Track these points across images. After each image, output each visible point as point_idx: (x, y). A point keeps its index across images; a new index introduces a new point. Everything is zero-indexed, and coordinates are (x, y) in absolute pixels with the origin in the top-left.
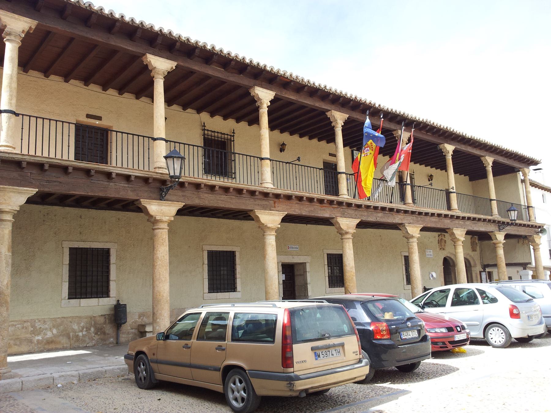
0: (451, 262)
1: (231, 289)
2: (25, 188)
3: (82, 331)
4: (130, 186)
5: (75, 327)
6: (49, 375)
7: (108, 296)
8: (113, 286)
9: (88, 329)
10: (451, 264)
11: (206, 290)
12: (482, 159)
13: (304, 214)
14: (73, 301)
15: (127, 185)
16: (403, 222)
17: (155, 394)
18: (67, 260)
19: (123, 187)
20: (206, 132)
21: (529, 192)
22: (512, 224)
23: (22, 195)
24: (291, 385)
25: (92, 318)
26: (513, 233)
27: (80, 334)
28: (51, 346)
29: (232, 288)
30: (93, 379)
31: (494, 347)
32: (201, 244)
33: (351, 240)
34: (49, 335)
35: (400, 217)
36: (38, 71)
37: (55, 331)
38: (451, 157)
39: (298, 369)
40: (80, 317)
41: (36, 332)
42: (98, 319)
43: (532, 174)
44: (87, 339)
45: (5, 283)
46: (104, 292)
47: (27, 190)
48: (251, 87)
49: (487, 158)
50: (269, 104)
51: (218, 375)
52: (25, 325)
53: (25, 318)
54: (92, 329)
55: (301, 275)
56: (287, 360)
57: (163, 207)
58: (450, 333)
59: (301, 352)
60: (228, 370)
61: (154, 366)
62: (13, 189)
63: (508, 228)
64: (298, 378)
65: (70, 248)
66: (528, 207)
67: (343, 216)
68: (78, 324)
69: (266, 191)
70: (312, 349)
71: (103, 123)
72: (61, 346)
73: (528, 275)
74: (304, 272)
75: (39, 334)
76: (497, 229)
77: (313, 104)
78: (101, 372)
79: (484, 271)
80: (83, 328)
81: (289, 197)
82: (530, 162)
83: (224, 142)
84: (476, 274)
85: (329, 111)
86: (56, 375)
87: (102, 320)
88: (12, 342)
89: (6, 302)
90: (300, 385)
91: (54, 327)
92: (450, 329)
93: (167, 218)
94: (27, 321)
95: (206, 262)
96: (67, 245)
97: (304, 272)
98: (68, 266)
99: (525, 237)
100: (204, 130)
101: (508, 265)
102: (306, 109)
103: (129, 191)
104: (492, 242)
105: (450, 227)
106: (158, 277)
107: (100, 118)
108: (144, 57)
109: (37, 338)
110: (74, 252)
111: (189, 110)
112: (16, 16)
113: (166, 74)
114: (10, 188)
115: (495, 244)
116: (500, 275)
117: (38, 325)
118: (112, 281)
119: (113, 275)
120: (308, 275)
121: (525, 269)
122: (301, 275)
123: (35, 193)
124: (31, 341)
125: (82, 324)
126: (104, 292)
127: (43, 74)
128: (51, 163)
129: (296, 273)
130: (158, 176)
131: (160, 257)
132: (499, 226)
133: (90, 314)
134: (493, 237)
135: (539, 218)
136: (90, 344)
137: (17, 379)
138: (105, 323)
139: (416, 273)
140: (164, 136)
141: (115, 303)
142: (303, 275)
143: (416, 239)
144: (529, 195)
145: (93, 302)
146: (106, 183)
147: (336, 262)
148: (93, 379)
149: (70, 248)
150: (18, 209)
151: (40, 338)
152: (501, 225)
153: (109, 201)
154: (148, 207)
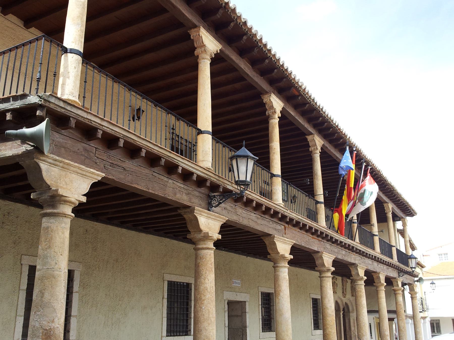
1: (183, 332)
2: (92, 170)
4: (185, 187)
11: (165, 333)
13: (303, 245)
15: (182, 186)
16: (357, 262)
19: (179, 187)
23: (85, 180)
32: (163, 272)
36: (18, 17)
47: (93, 173)
55: (237, 316)
62: (79, 168)
63: (406, 276)
65: (30, 266)
74: (242, 313)
77: (303, 124)
84: (354, 320)
85: (311, 134)
97: (242, 313)
98: (25, 292)
101: (369, 312)
102: (293, 127)
103: (184, 194)
104: (393, 288)
105: (378, 271)
106: (206, 316)
108: (193, 30)
114: (75, 167)
115: (395, 290)
116: (400, 322)
118: (74, 316)
122: (237, 316)
123: (100, 178)
127: (23, 22)
128: (129, 140)
131: (209, 288)
132: (399, 273)
134: (394, 283)
142: (241, 316)
143: (363, 282)
146: (166, 179)
147: (268, 302)
149: (30, 266)
153: (157, 203)
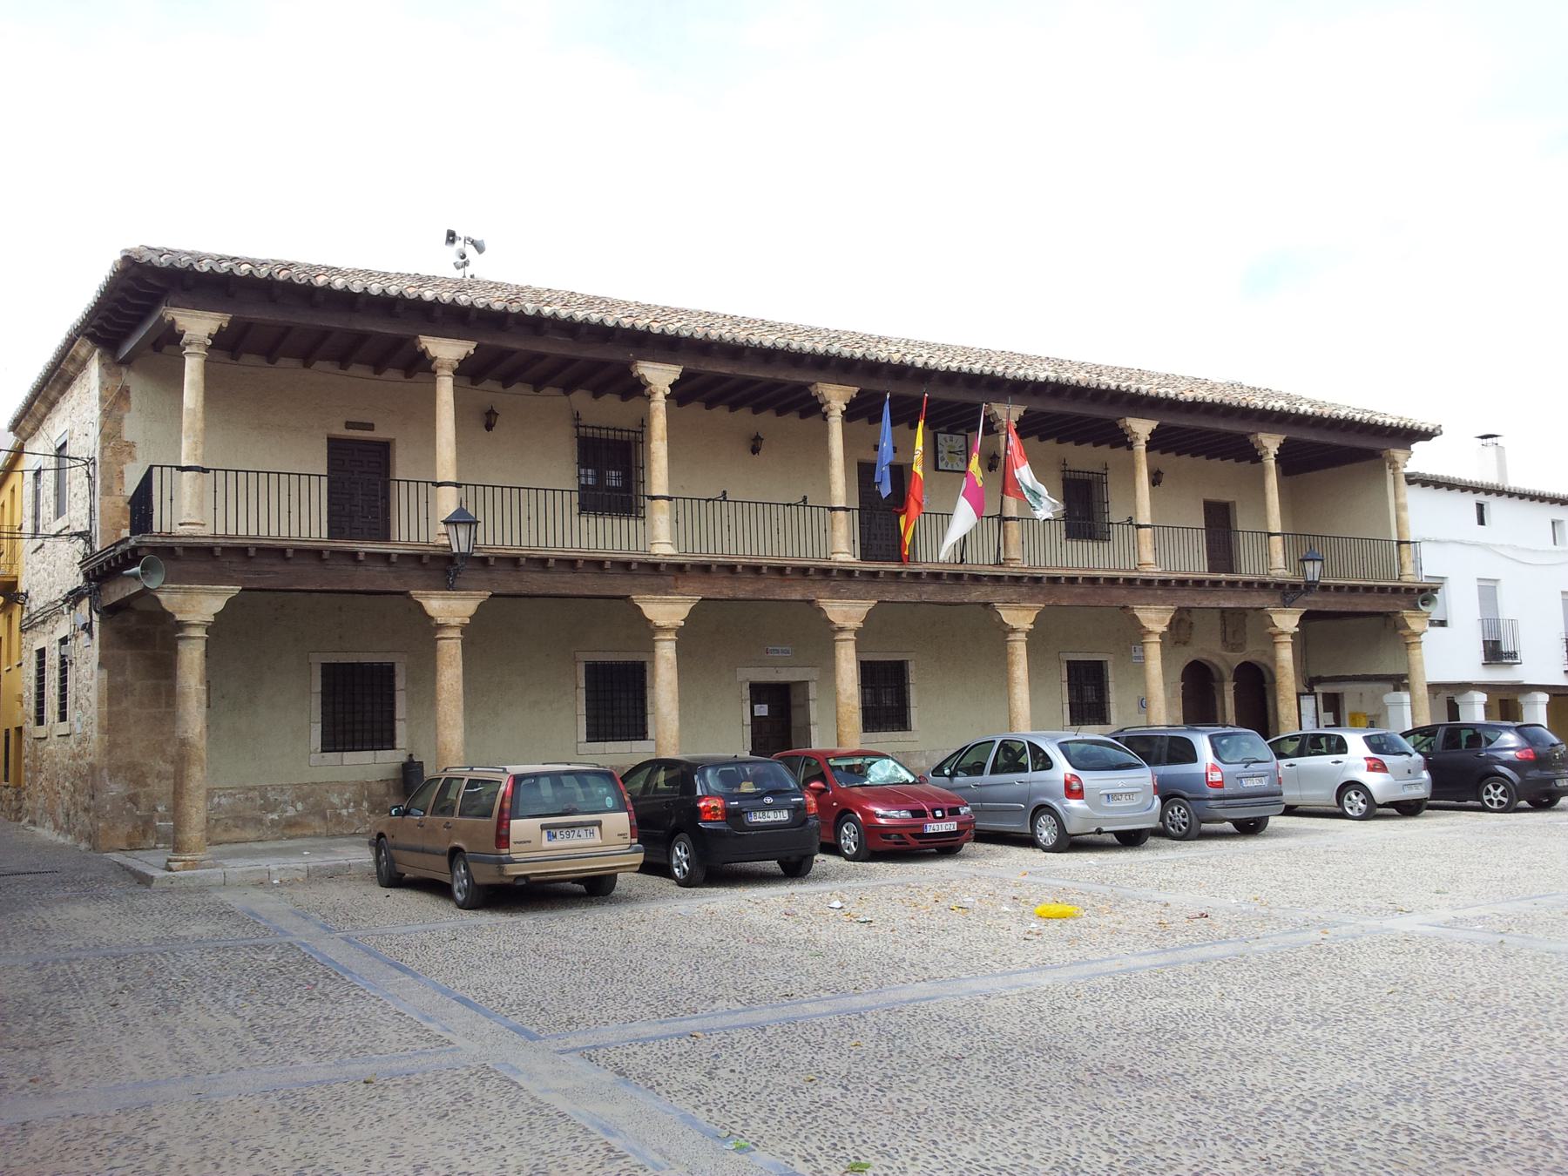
0: (1214, 670)
3: (347, 807)
5: (335, 800)
6: (264, 866)
7: (393, 748)
8: (401, 729)
9: (358, 804)
10: (1216, 676)
12: (1252, 439)
14: (332, 757)
17: (398, 895)
18: (317, 687)
20: (582, 430)
21: (1404, 507)
22: (1310, 586)
24: (501, 869)
25: (364, 785)
26: (1320, 607)
27: (344, 812)
28: (294, 832)
29: (1406, 676)
30: (333, 875)
31: (1046, 850)
33: (852, 644)
34: (291, 812)
35: (983, 589)
37: (300, 806)
38: (1143, 448)
39: (515, 851)
40: (343, 784)
41: (269, 807)
42: (375, 786)
43: (1420, 458)
44: (356, 822)
45: (197, 730)
46: (388, 742)
48: (632, 363)
49: (1261, 436)
50: (668, 391)
51: (445, 860)
52: (251, 794)
53: (251, 784)
54: (365, 804)
56: (502, 839)
57: (452, 602)
58: (918, 821)
59: (520, 827)
60: (455, 853)
61: (393, 852)
64: (512, 861)
66: (1399, 543)
67: (836, 595)
68: (341, 794)
69: (651, 559)
70: (543, 827)
71: (379, 434)
72: (310, 832)
73: (1401, 704)
75: (272, 812)
76: (1278, 600)
78: (343, 867)
79: (1311, 693)
80: (348, 802)
81: (705, 568)
82: (1408, 436)
83: (628, 443)
86: (273, 868)
87: (382, 789)
88: (230, 822)
89: (201, 759)
90: (512, 870)
91: (299, 798)
92: (918, 813)
93: (458, 620)
94: (254, 788)
95: (582, 684)
96: (318, 659)
99: (1386, 616)
100: (577, 427)
107: (370, 427)
109: (271, 816)
110: (329, 670)
111: (548, 390)
112: (199, 313)
113: (456, 365)
115: (1274, 635)
117: (271, 795)
119: (400, 712)
120: (813, 706)
121: (1397, 689)
124: (259, 822)
125: (347, 796)
126: (388, 742)
129: (794, 701)
130: (440, 551)
132: (1285, 594)
133: (360, 777)
135: (1430, 564)
136: (362, 830)
137: (219, 870)
138: (387, 795)
139: (1019, 703)
140: (453, 479)
141: (405, 759)
144: (1403, 514)
145: (366, 757)
148: (333, 875)
150: (212, 619)
151: (275, 816)
152: (1287, 592)
154: (424, 602)
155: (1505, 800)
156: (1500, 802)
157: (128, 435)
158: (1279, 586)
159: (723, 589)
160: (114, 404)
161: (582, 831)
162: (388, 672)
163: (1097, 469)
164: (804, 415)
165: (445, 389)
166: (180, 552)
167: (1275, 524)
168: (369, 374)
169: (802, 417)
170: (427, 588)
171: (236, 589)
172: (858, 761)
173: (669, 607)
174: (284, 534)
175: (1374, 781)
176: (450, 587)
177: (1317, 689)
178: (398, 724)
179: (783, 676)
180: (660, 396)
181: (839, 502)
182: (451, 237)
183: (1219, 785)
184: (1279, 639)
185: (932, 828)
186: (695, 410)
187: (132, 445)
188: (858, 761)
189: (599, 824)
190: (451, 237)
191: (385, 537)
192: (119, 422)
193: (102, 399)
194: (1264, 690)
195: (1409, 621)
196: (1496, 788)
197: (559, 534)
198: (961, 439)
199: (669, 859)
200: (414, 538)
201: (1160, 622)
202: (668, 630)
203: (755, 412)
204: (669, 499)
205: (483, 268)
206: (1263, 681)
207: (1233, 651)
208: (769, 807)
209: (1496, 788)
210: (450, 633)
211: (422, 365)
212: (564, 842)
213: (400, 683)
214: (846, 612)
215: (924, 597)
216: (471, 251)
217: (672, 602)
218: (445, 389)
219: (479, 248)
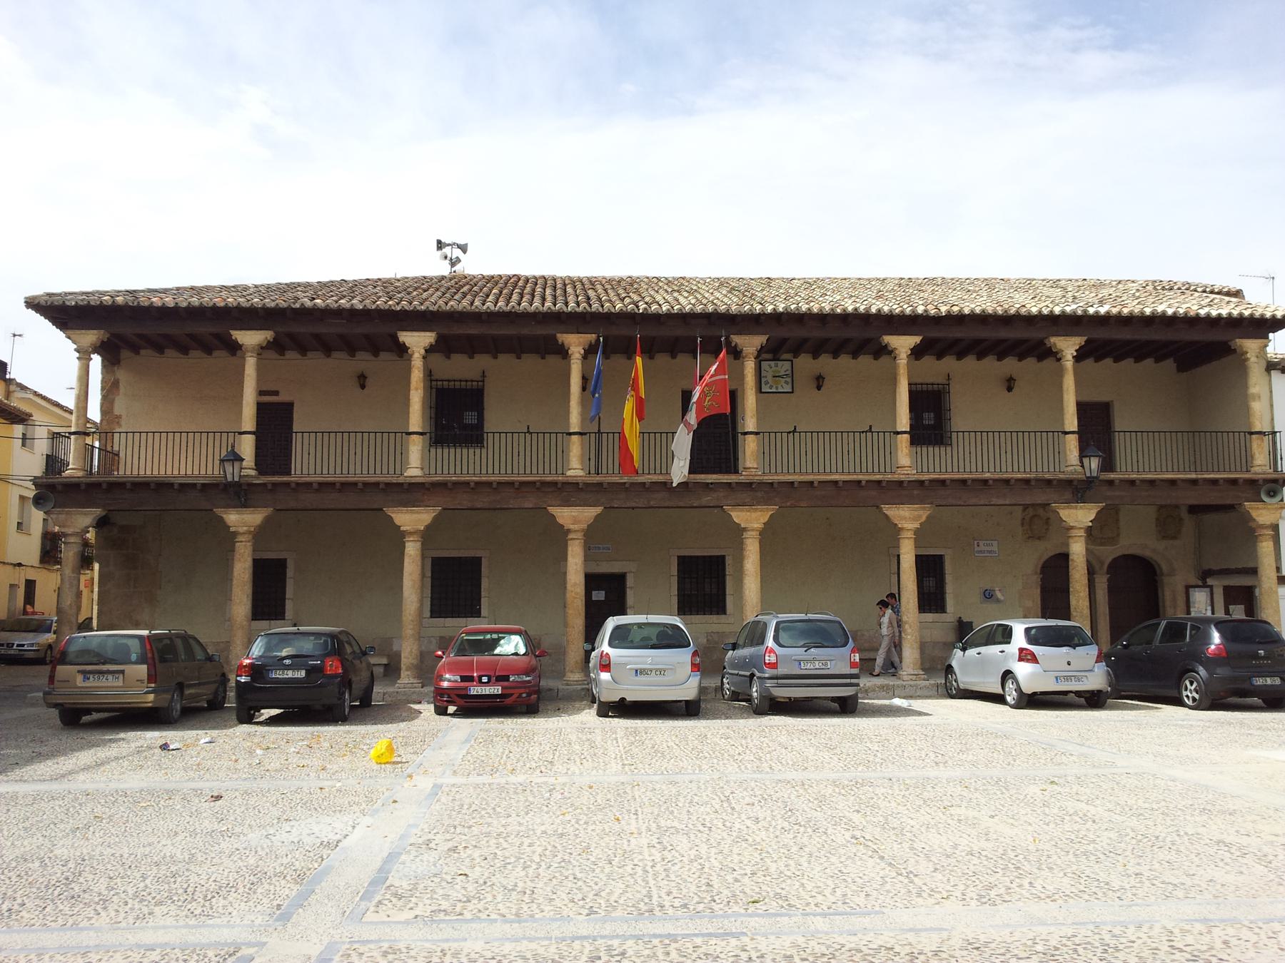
7: (725, 613)
8: (289, 605)
18: (674, 571)
49: (1053, 340)
92: (464, 679)
99: (1231, 507)
107: (276, 393)
110: (684, 562)
155: (1197, 696)
156: (1194, 700)
157: (117, 411)
158: (1069, 482)
159: (464, 500)
160: (108, 391)
161: (110, 677)
162: (477, 562)
163: (941, 380)
164: (1040, 358)
165: (250, 365)
166: (60, 488)
167: (575, 422)
168: (277, 356)
169: (1096, 361)
170: (228, 506)
171: (599, 510)
172: (495, 636)
173: (415, 516)
174: (162, 472)
175: (1023, 671)
176: (245, 506)
177: (1210, 581)
178: (287, 602)
179: (615, 568)
180: (416, 355)
181: (575, 428)
182: (440, 245)
183: (773, 666)
184: (1073, 533)
185: (476, 690)
186: (1089, 363)
187: (119, 417)
188: (495, 636)
189: (122, 672)
190: (440, 245)
191: (289, 473)
192: (112, 403)
193: (103, 389)
194: (1156, 581)
195: (1254, 514)
196: (1192, 683)
197: (833, 462)
198: (787, 365)
199: (1180, 693)
200: (210, 472)
201: (914, 519)
202: (411, 533)
203: (1000, 359)
204: (757, 433)
205: (472, 266)
206: (1155, 573)
207: (1102, 544)
208: (288, 667)
209: (1192, 683)
210: (72, 540)
211: (235, 348)
212: (93, 682)
213: (290, 572)
214: (242, 520)
215: (652, 503)
216: (457, 253)
217: (418, 513)
218: (250, 365)
219: (464, 248)
